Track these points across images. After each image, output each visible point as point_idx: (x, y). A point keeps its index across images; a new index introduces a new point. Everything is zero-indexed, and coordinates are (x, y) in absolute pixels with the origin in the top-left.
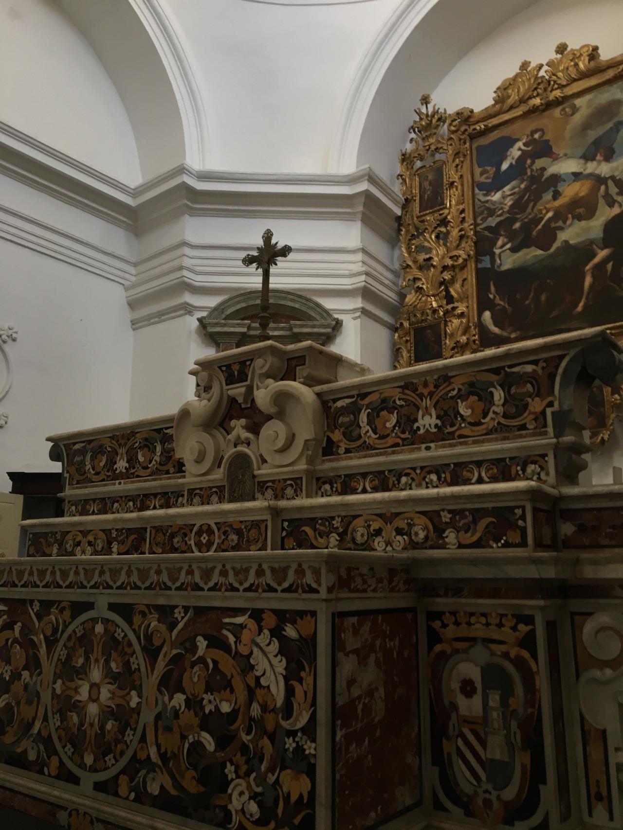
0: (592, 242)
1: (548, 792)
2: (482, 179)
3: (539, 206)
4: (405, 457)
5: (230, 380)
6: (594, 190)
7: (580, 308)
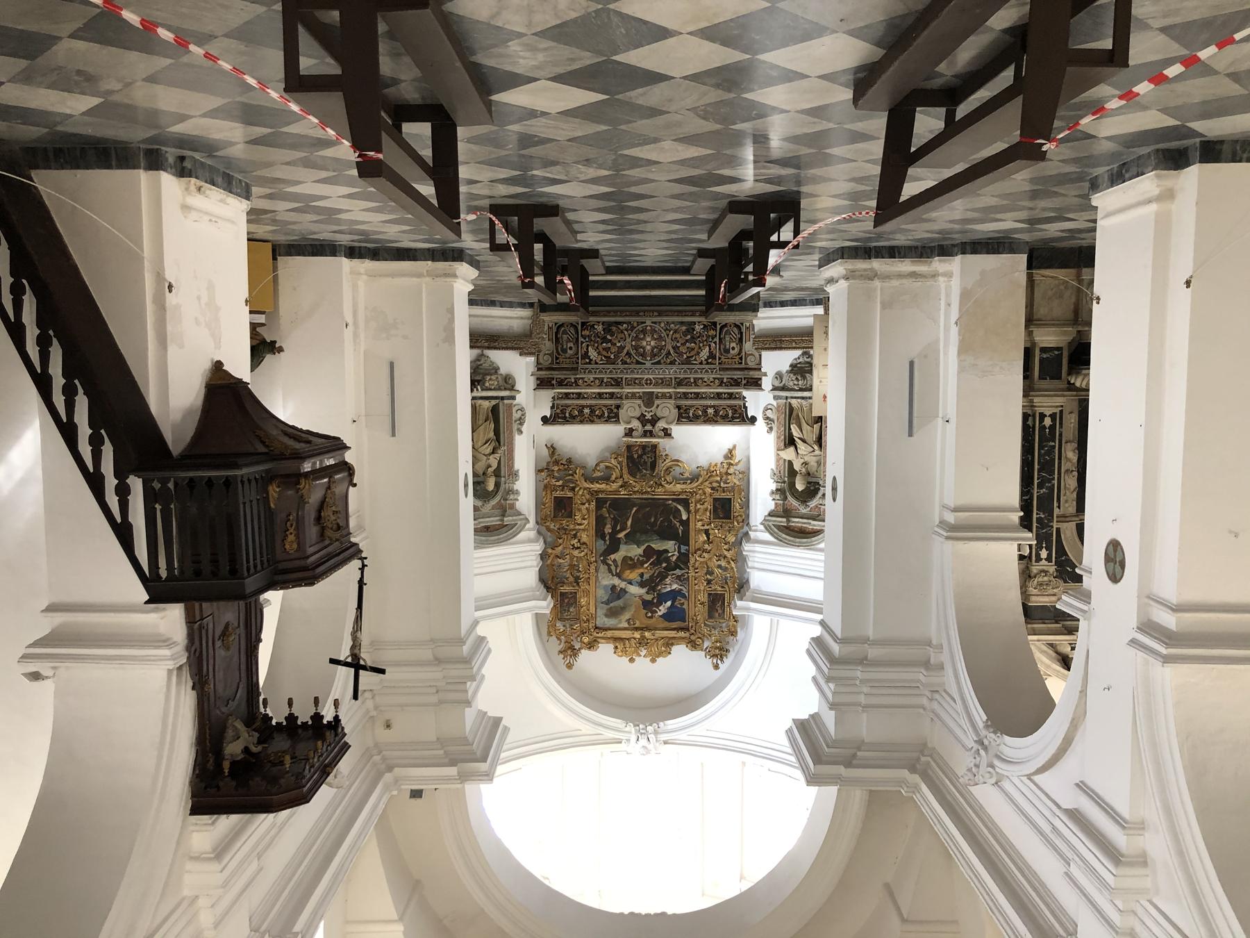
0: (626, 543)
1: (555, 330)
2: (683, 601)
3: (652, 572)
4: (593, 402)
5: (651, 432)
6: (622, 571)
7: (635, 509)
